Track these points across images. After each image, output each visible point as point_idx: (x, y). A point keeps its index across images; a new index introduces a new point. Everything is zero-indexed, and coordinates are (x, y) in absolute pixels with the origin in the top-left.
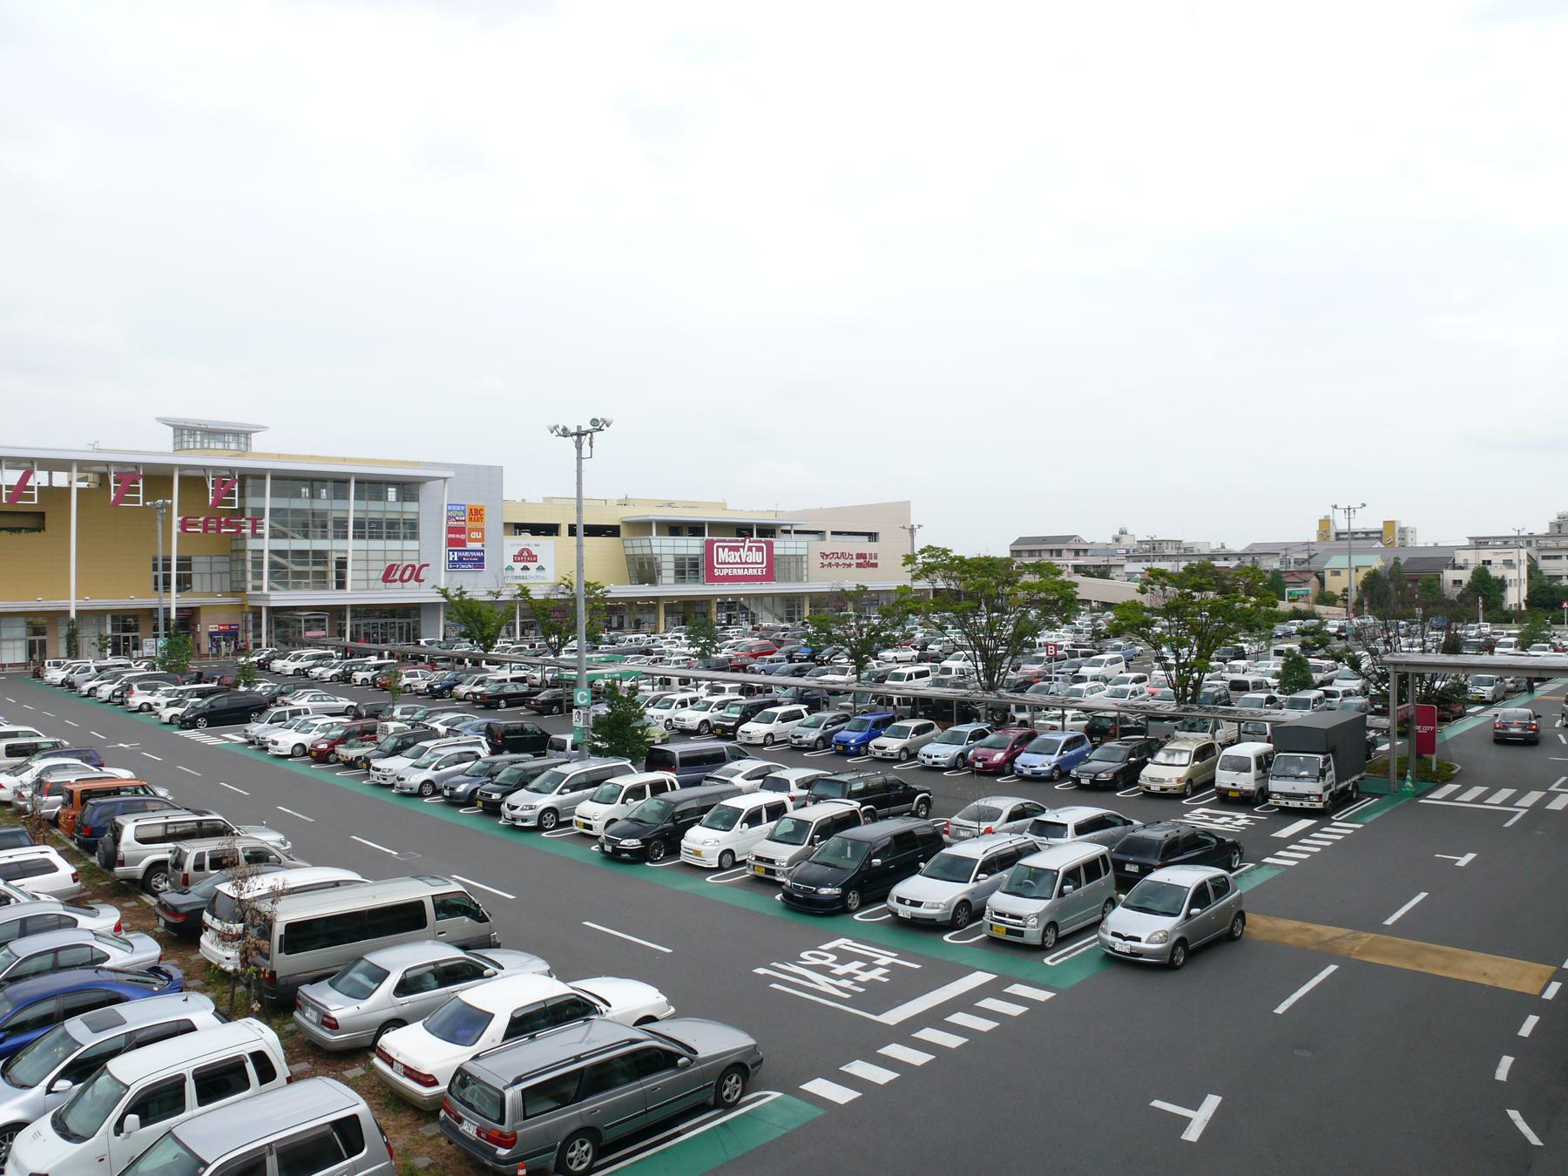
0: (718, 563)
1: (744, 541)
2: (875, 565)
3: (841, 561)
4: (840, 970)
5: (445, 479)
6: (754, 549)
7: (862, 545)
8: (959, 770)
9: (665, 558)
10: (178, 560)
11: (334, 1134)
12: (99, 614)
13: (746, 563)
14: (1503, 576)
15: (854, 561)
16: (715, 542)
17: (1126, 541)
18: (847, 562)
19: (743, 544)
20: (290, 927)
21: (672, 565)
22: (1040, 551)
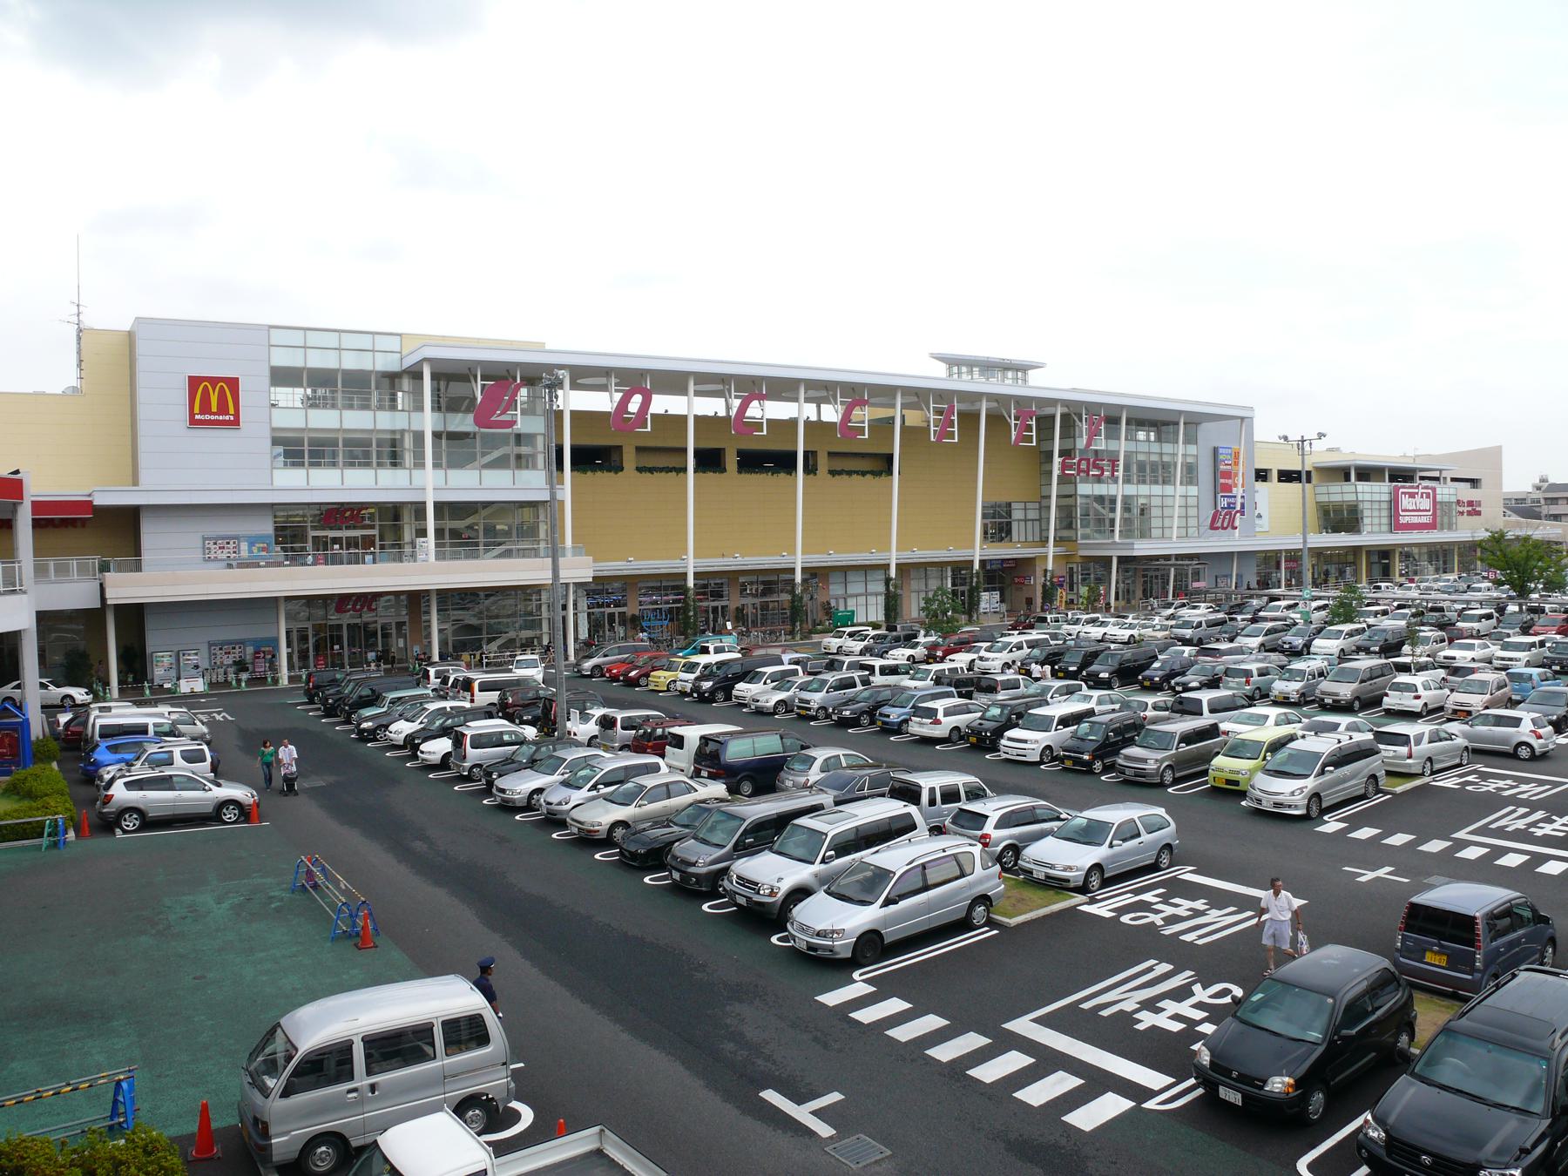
2: (1479, 513)
5: (1242, 419)
7: (1466, 492)
8: (955, 744)
10: (983, 507)
11: (1469, 977)
12: (923, 567)
13: (1420, 510)
19: (1417, 491)
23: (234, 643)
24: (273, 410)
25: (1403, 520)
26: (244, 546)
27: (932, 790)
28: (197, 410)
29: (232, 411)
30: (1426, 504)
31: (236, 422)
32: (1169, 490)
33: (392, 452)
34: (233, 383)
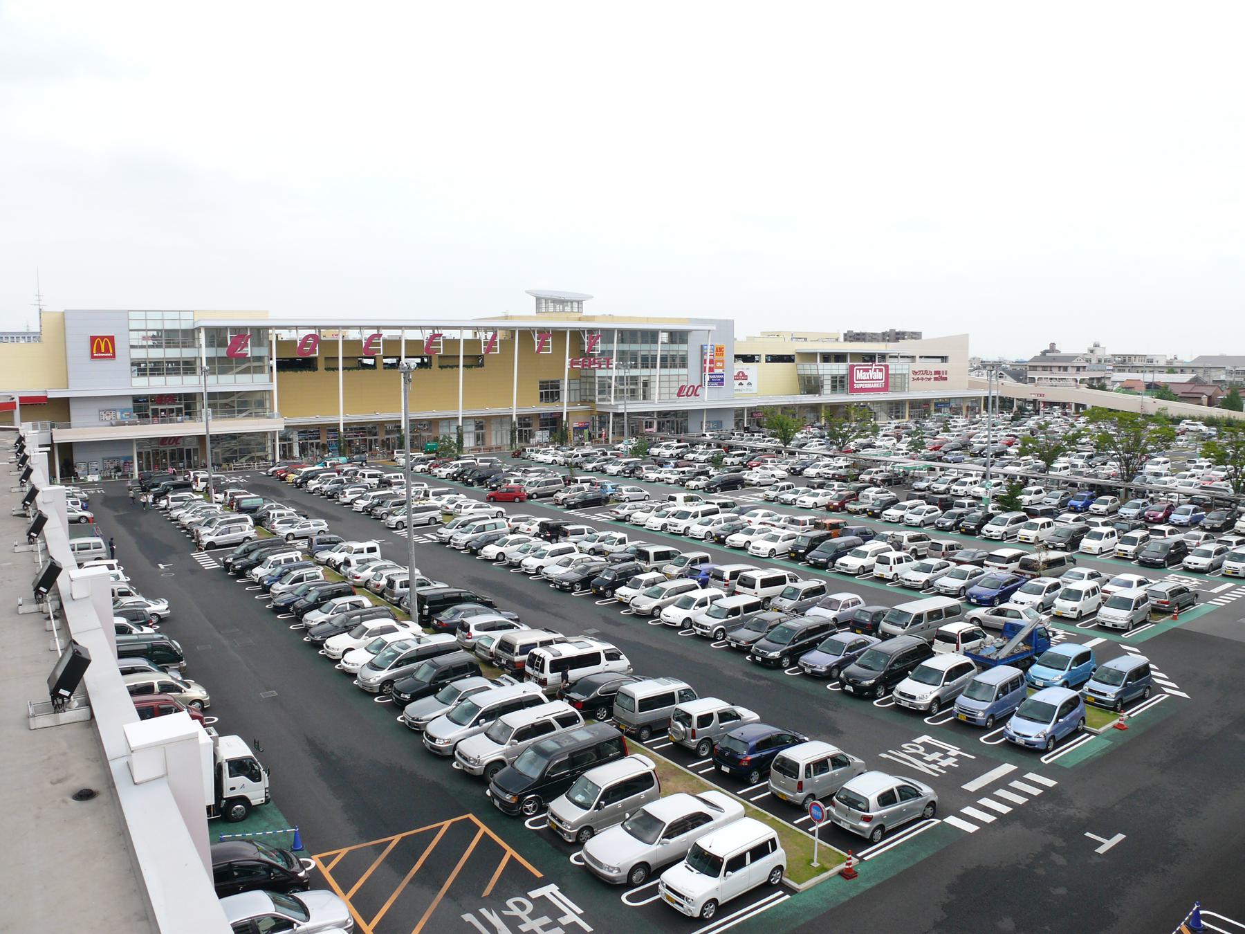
1: (872, 365)
2: (945, 379)
3: (925, 376)
4: (929, 758)
7: (936, 365)
9: (826, 377)
13: (873, 380)
15: (933, 376)
17: (1098, 352)
18: (928, 377)
20: (521, 646)
21: (830, 382)
22: (1051, 367)
23: (114, 458)
24: (132, 350)
25: (856, 386)
26: (119, 414)
27: (274, 515)
28: (95, 351)
29: (111, 351)
30: (879, 375)
31: (114, 357)
32: (653, 371)
33: (188, 367)
34: (112, 339)
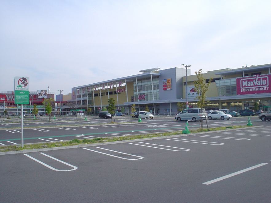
0: (242, 87)
6: (261, 79)
13: (257, 85)
14: (243, 66)
16: (241, 79)
19: (255, 78)
